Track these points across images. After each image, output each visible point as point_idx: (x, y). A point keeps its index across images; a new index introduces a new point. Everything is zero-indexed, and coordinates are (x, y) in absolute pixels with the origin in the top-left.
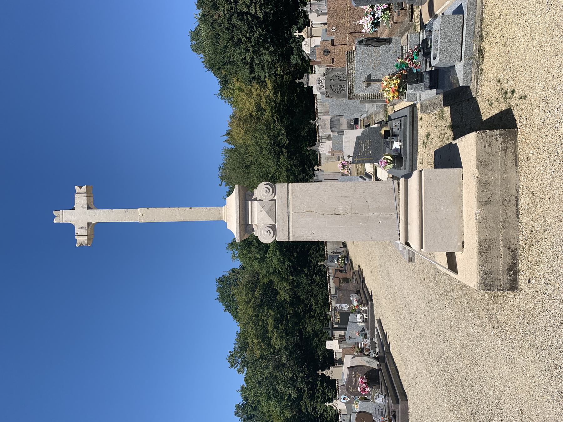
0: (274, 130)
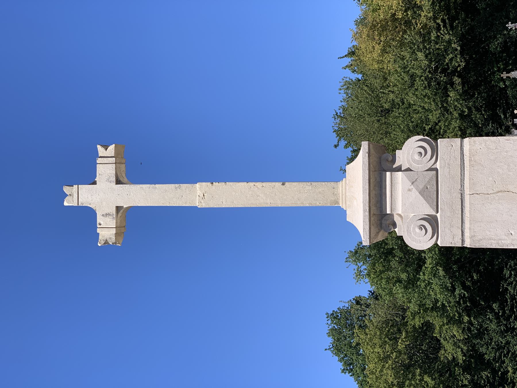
0: (437, 43)
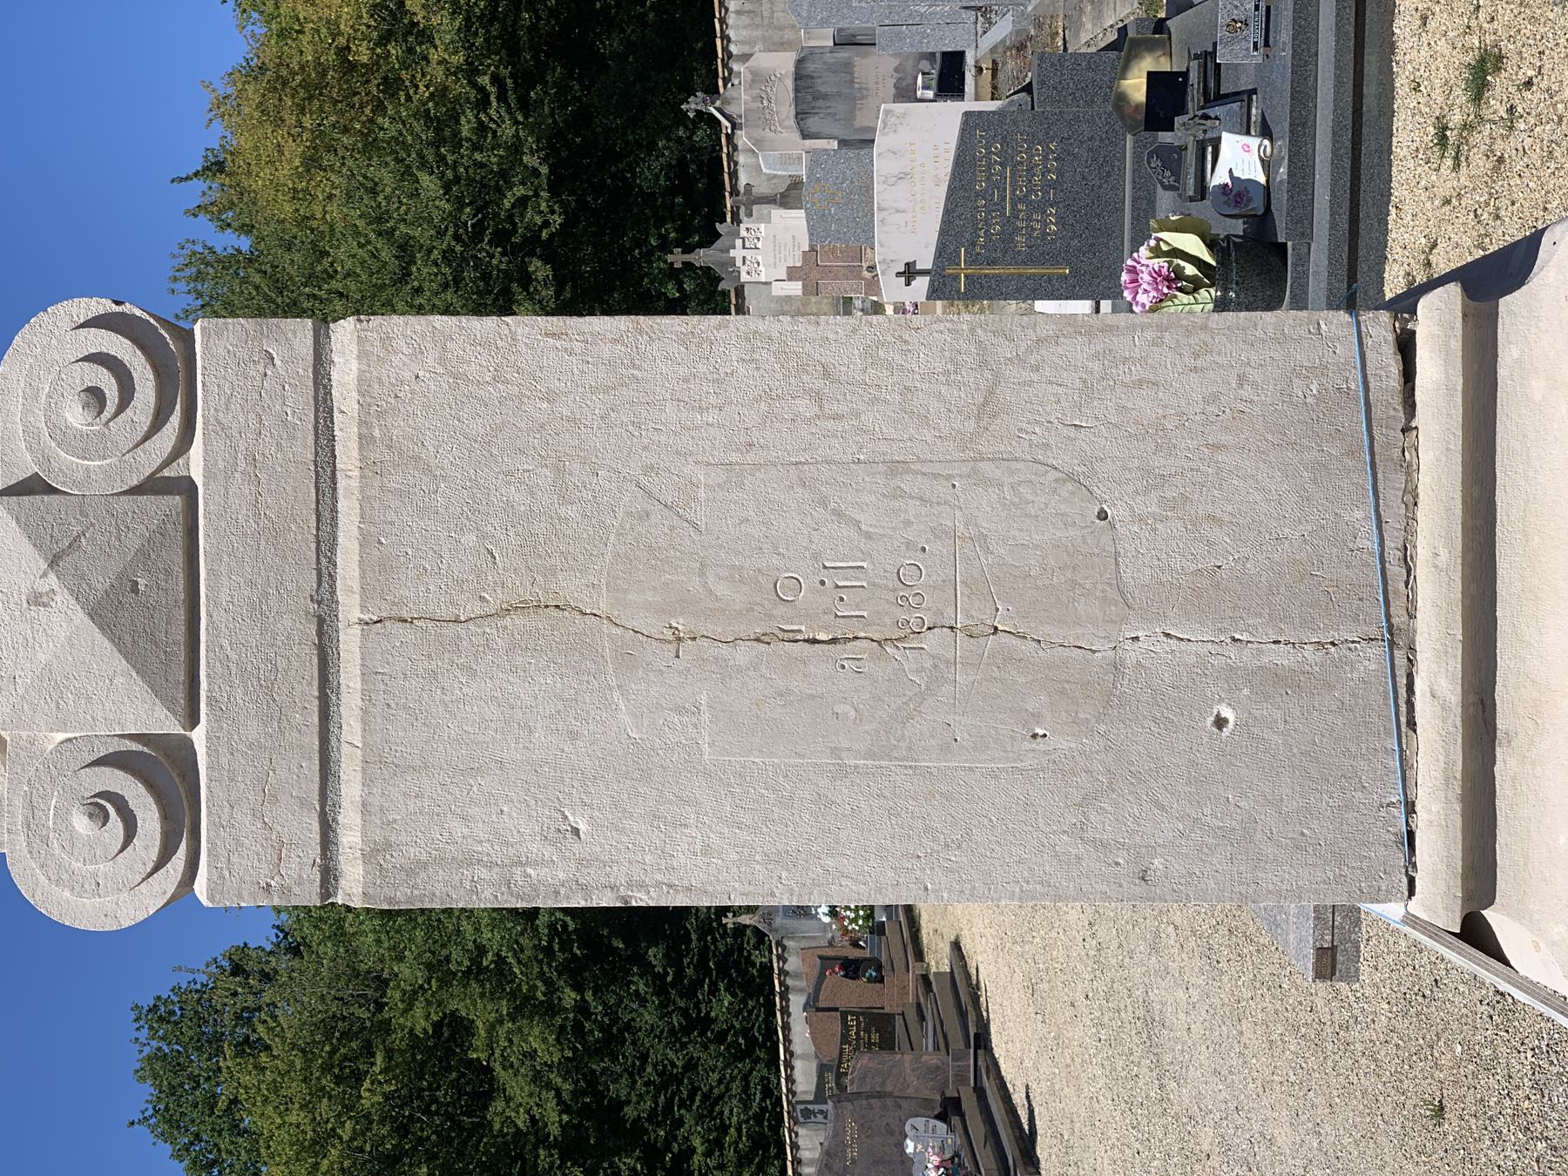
0: (476, 147)
